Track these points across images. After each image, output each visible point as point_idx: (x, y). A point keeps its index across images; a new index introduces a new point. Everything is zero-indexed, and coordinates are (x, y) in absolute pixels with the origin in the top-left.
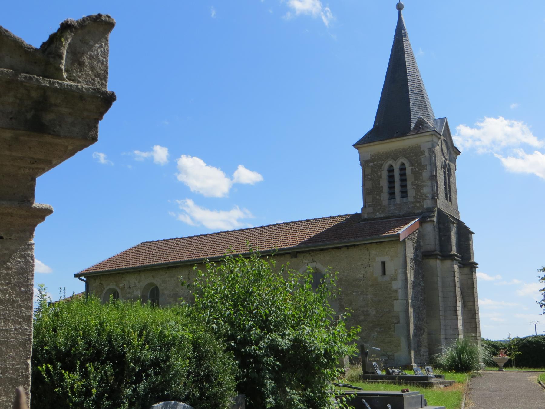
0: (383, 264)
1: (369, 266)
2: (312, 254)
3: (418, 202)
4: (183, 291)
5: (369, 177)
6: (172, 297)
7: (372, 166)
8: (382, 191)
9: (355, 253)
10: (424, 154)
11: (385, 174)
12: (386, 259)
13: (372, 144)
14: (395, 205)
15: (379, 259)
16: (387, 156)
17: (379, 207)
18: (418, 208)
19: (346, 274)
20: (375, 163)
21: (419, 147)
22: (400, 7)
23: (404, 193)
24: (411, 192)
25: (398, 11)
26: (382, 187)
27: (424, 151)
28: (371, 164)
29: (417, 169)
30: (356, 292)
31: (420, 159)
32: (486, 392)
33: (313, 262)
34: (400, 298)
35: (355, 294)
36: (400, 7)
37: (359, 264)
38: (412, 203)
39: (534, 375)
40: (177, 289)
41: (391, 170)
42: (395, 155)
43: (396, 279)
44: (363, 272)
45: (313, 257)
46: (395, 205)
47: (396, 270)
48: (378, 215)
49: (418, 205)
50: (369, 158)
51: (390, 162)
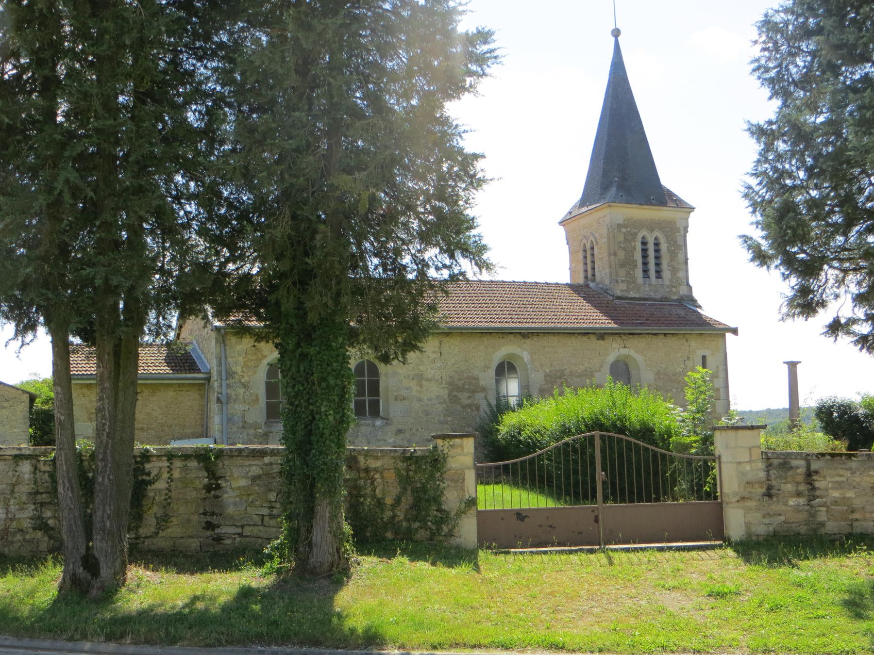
0: (704, 358)
1: (688, 358)
2: (624, 337)
3: (674, 287)
4: (433, 372)
5: (622, 245)
6: (413, 379)
7: (625, 233)
8: (636, 265)
9: (671, 342)
10: (679, 232)
11: (639, 247)
12: (707, 353)
13: (629, 205)
14: (650, 285)
15: (700, 353)
16: (640, 224)
17: (633, 285)
18: (675, 294)
19: (664, 366)
20: (629, 229)
21: (675, 223)
22: (616, 33)
23: (659, 273)
24: (666, 274)
25: (613, 39)
26: (636, 261)
27: (679, 228)
28: (624, 230)
29: (673, 248)
30: (676, 388)
31: (676, 237)
32: (217, 432)
33: (625, 347)
34: (721, 398)
35: (674, 390)
36: (616, 33)
37: (679, 355)
38: (669, 287)
39: (836, 469)
40: (422, 368)
41: (644, 243)
42: (652, 226)
43: (717, 377)
44: (683, 366)
45: (625, 342)
46: (650, 285)
47: (718, 367)
48: (632, 294)
49: (674, 290)
50: (621, 222)
51: (644, 233)
